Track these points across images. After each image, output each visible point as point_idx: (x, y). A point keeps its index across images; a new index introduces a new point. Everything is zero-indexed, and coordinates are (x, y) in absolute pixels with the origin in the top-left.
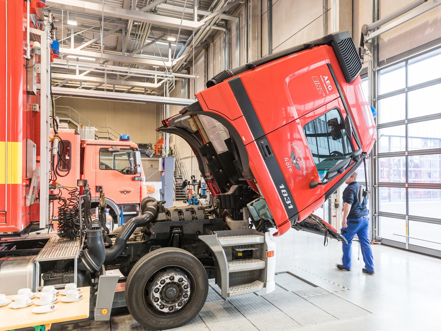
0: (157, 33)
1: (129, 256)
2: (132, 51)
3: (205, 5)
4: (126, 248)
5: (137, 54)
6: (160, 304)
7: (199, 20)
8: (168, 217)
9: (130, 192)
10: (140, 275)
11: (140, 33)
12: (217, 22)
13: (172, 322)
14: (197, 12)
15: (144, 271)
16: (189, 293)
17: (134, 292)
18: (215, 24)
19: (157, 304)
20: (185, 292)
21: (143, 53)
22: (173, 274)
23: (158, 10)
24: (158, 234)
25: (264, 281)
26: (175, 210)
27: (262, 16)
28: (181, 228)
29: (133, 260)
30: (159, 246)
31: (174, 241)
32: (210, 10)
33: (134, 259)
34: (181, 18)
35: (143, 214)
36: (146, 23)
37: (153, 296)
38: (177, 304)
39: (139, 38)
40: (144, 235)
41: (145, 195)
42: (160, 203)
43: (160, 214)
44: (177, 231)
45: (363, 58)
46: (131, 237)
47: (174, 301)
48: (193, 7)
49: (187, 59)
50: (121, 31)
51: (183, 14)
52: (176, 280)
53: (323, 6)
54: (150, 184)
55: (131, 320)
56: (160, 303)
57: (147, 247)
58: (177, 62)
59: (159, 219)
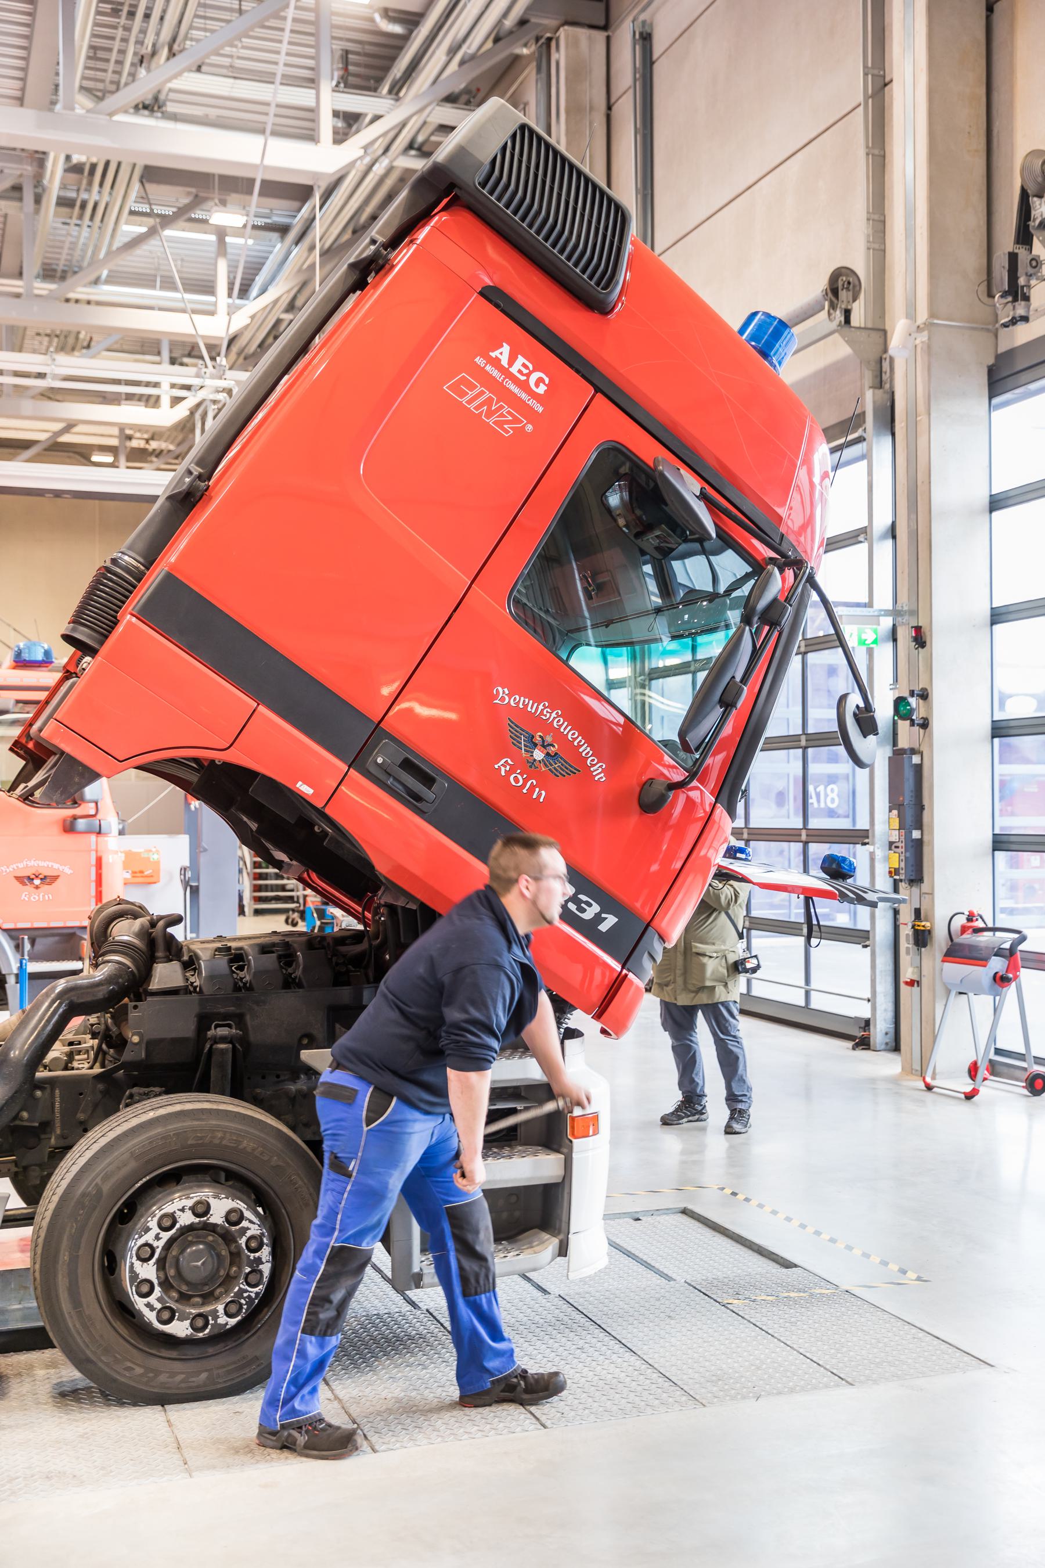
0: (168, 198)
1: (46, 1126)
2: (63, 278)
3: (367, 66)
4: (32, 1096)
5: (85, 286)
6: (158, 1306)
7: (340, 137)
8: (192, 979)
9: (55, 878)
10: (84, 1195)
11: (94, 196)
12: (420, 139)
13: (204, 1376)
14: (330, 99)
15: (98, 1180)
16: (266, 1269)
17: (64, 1257)
18: (411, 146)
19: (149, 1305)
20: (250, 1263)
21: (114, 279)
22: (205, 1193)
23: (172, 96)
24: (151, 1045)
25: (559, 1233)
26: (218, 950)
27: (609, 108)
28: (239, 1020)
29: (62, 1143)
30: (157, 1089)
31: (214, 1073)
32: (390, 92)
33: (63, 1137)
34: (262, 132)
35: (96, 966)
36: (119, 164)
37: (134, 1276)
38: (221, 1308)
39: (92, 218)
40: (100, 1047)
41: (116, 888)
42: (161, 923)
43: (160, 965)
44: (223, 1031)
45: (1027, 298)
46: (52, 1055)
47: (209, 1297)
48: (312, 82)
49: (294, 298)
50: (17, 188)
51: (272, 110)
52: (217, 1217)
53: (865, 67)
54: (139, 843)
55: (55, 1367)
56: (159, 1300)
57: (112, 1091)
58: (253, 317)
59: (155, 985)
